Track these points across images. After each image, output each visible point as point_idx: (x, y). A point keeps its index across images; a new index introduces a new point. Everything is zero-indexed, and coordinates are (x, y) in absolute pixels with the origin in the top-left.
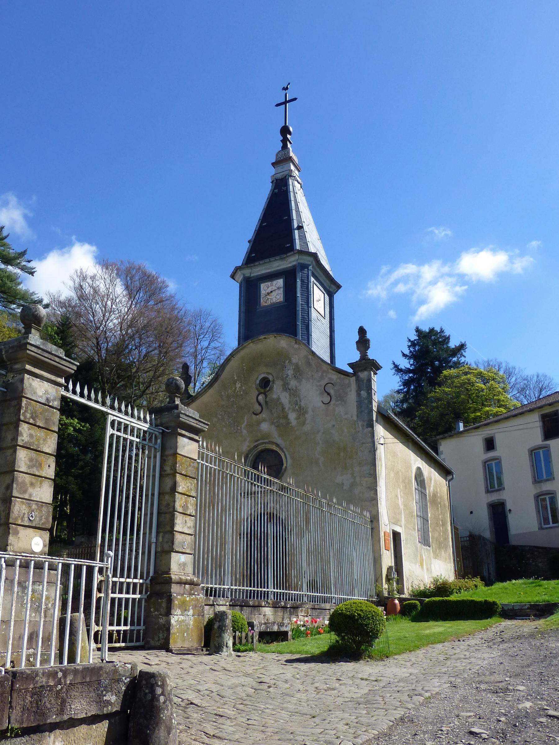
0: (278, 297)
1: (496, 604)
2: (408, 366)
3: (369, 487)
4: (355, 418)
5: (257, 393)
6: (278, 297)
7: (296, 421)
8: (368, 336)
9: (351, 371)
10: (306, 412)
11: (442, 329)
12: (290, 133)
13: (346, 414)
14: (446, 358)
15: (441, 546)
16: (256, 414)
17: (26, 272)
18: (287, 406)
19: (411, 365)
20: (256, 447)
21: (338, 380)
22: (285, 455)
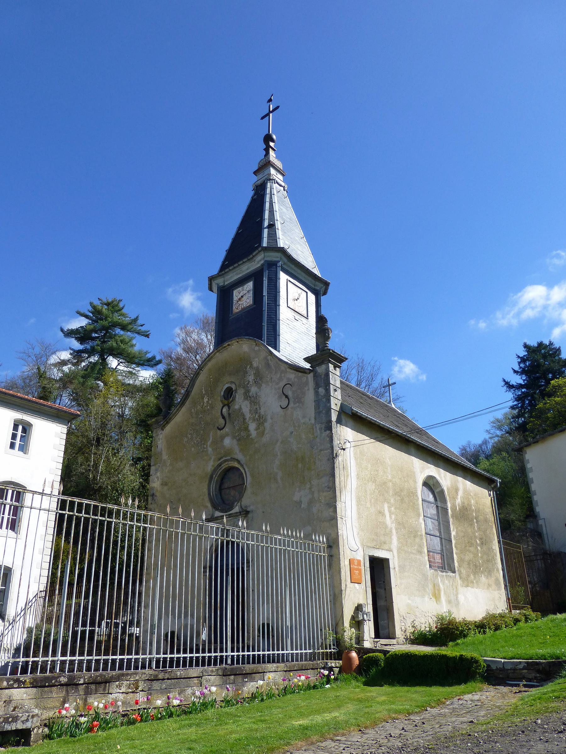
0: (248, 301)
1: (477, 662)
2: (521, 382)
3: (328, 504)
4: (313, 421)
5: (222, 405)
6: (248, 301)
7: (256, 432)
8: (329, 325)
9: (307, 366)
10: (265, 420)
11: (550, 342)
12: (273, 141)
13: (304, 417)
14: (559, 369)
15: (477, 569)
16: (220, 429)
17: (142, 335)
18: (248, 416)
19: (524, 380)
20: (220, 465)
21: (296, 380)
22: (245, 471)
